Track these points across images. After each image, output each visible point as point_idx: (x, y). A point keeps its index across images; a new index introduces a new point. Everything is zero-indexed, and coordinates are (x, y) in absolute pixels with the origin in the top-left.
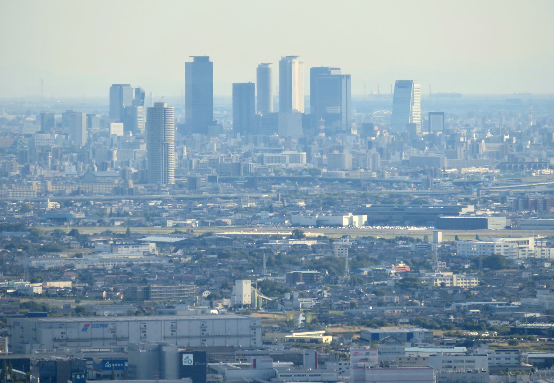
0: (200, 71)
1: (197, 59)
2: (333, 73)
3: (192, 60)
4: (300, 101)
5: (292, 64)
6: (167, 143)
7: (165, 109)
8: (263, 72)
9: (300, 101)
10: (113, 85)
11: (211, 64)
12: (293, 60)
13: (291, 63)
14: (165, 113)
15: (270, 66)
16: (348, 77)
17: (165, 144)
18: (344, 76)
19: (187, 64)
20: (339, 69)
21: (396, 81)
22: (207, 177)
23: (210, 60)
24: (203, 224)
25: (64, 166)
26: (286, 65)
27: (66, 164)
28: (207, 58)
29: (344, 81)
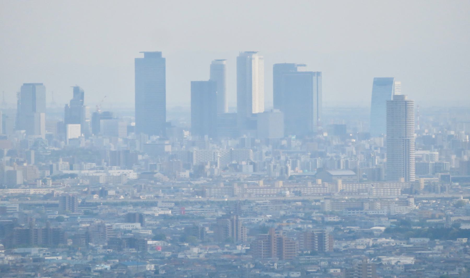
0: (151, 67)
1: (148, 55)
2: (300, 69)
3: (142, 56)
4: (261, 101)
5: (253, 61)
6: (408, 139)
7: (406, 102)
8: (218, 69)
9: (261, 101)
10: (24, 84)
11: (164, 60)
12: (254, 56)
13: (251, 59)
14: (406, 106)
15: (224, 63)
16: (319, 74)
17: (406, 140)
18: (314, 73)
19: (137, 61)
20: (305, 65)
21: (375, 78)
22: (440, 177)
23: (163, 56)
24: (361, 228)
25: (241, 166)
26: (244, 63)
27: (244, 163)
28: (158, 54)
29: (315, 78)
